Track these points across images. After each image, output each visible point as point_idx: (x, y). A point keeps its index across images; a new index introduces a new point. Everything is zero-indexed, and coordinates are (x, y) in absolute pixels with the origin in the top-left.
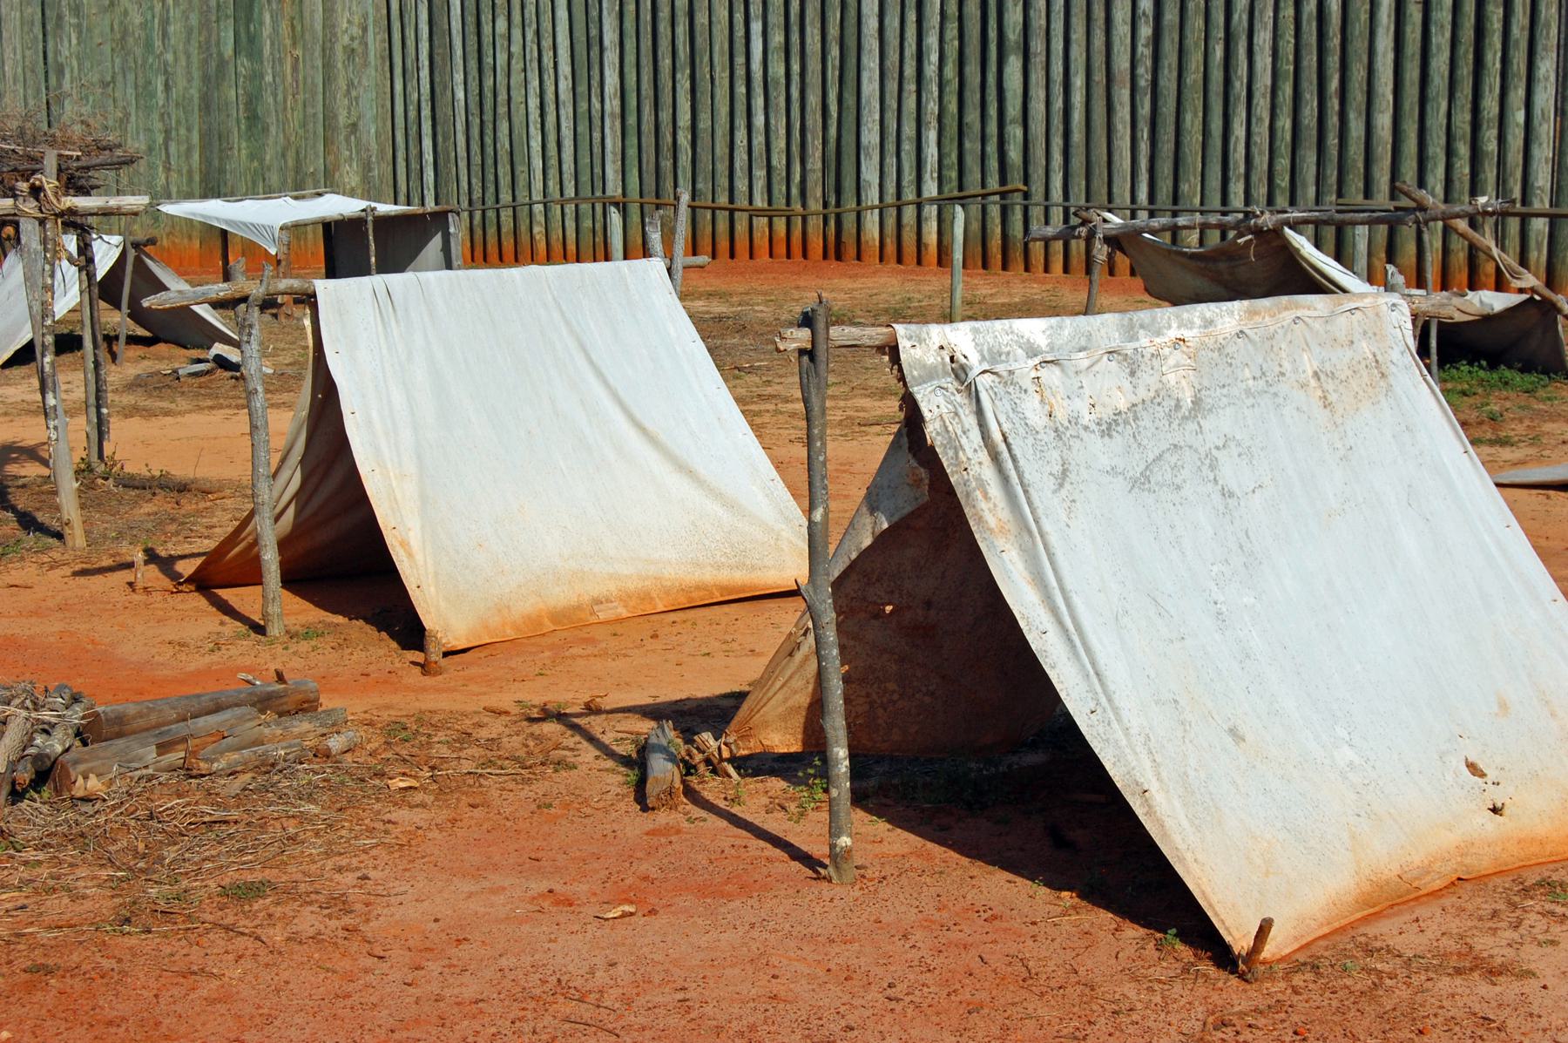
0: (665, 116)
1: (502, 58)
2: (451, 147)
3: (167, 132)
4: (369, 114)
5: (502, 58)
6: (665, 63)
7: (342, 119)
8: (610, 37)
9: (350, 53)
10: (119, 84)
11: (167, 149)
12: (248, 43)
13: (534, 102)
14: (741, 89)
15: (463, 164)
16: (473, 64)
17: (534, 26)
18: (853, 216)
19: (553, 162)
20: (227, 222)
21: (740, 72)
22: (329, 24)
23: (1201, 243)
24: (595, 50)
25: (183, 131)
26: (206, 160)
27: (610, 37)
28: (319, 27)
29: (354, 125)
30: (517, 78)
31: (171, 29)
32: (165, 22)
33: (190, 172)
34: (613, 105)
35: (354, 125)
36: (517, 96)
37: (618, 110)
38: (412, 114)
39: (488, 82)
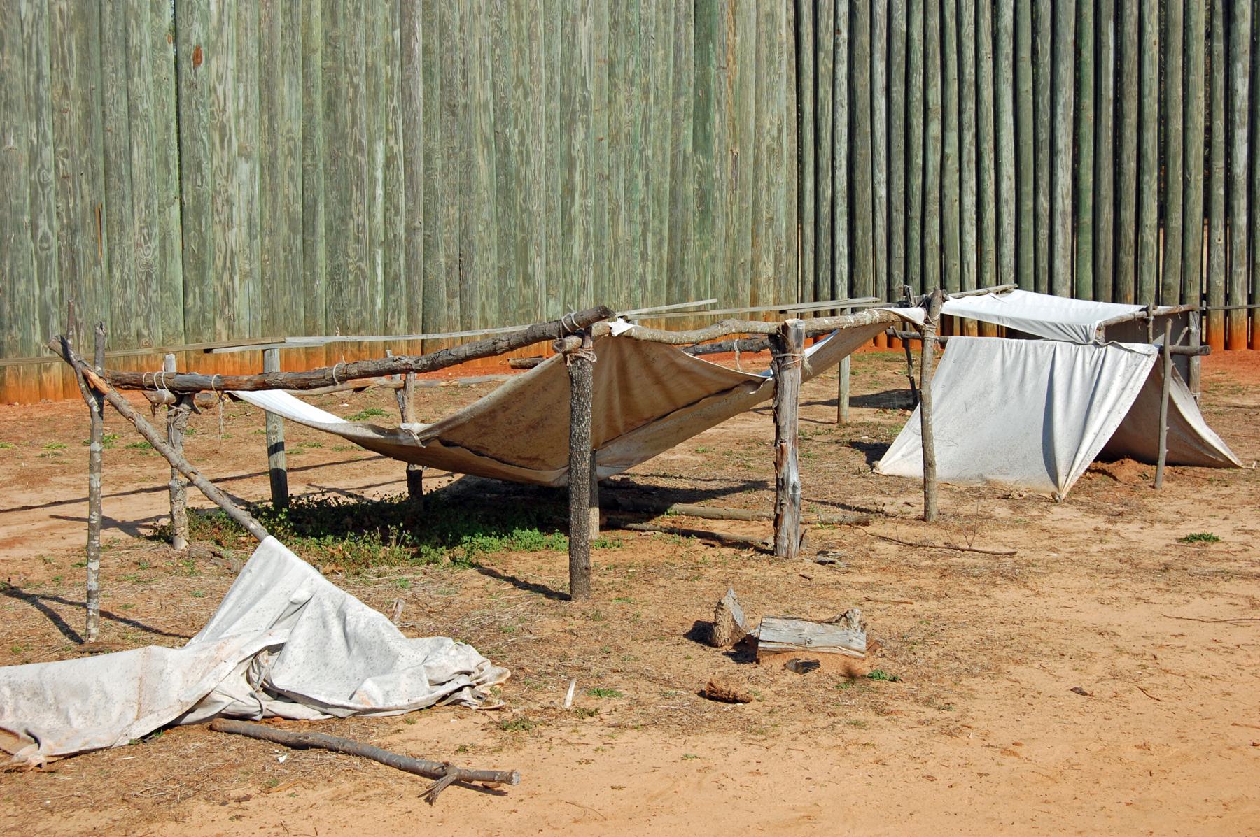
0: (1128, 215)
1: (934, 159)
2: (870, 241)
3: (645, 224)
4: (783, 209)
5: (934, 159)
6: (1130, 166)
7: (764, 216)
8: (1064, 140)
9: (771, 150)
10: (614, 179)
11: (645, 240)
12: (702, 142)
13: (970, 201)
14: (1219, 192)
15: (882, 257)
16: (899, 165)
17: (973, 130)
18: (1221, 314)
19: (991, 256)
20: (1012, 320)
21: (1219, 174)
22: (758, 127)
23: (566, 310)
24: (1044, 155)
25: (656, 224)
26: (672, 250)
27: (1064, 140)
28: (752, 127)
29: (772, 219)
30: (952, 178)
31: (652, 126)
32: (646, 121)
33: (661, 261)
34: (1064, 203)
35: (772, 219)
36: (952, 193)
37: (1069, 209)
38: (825, 209)
39: (917, 181)
